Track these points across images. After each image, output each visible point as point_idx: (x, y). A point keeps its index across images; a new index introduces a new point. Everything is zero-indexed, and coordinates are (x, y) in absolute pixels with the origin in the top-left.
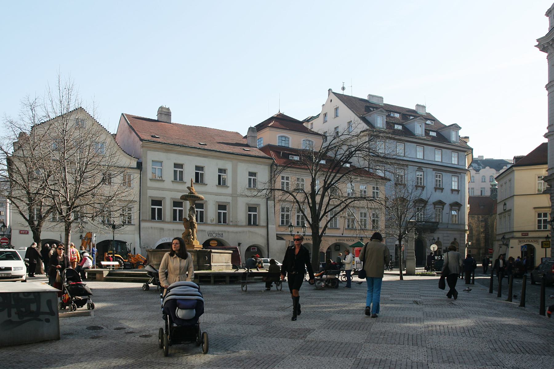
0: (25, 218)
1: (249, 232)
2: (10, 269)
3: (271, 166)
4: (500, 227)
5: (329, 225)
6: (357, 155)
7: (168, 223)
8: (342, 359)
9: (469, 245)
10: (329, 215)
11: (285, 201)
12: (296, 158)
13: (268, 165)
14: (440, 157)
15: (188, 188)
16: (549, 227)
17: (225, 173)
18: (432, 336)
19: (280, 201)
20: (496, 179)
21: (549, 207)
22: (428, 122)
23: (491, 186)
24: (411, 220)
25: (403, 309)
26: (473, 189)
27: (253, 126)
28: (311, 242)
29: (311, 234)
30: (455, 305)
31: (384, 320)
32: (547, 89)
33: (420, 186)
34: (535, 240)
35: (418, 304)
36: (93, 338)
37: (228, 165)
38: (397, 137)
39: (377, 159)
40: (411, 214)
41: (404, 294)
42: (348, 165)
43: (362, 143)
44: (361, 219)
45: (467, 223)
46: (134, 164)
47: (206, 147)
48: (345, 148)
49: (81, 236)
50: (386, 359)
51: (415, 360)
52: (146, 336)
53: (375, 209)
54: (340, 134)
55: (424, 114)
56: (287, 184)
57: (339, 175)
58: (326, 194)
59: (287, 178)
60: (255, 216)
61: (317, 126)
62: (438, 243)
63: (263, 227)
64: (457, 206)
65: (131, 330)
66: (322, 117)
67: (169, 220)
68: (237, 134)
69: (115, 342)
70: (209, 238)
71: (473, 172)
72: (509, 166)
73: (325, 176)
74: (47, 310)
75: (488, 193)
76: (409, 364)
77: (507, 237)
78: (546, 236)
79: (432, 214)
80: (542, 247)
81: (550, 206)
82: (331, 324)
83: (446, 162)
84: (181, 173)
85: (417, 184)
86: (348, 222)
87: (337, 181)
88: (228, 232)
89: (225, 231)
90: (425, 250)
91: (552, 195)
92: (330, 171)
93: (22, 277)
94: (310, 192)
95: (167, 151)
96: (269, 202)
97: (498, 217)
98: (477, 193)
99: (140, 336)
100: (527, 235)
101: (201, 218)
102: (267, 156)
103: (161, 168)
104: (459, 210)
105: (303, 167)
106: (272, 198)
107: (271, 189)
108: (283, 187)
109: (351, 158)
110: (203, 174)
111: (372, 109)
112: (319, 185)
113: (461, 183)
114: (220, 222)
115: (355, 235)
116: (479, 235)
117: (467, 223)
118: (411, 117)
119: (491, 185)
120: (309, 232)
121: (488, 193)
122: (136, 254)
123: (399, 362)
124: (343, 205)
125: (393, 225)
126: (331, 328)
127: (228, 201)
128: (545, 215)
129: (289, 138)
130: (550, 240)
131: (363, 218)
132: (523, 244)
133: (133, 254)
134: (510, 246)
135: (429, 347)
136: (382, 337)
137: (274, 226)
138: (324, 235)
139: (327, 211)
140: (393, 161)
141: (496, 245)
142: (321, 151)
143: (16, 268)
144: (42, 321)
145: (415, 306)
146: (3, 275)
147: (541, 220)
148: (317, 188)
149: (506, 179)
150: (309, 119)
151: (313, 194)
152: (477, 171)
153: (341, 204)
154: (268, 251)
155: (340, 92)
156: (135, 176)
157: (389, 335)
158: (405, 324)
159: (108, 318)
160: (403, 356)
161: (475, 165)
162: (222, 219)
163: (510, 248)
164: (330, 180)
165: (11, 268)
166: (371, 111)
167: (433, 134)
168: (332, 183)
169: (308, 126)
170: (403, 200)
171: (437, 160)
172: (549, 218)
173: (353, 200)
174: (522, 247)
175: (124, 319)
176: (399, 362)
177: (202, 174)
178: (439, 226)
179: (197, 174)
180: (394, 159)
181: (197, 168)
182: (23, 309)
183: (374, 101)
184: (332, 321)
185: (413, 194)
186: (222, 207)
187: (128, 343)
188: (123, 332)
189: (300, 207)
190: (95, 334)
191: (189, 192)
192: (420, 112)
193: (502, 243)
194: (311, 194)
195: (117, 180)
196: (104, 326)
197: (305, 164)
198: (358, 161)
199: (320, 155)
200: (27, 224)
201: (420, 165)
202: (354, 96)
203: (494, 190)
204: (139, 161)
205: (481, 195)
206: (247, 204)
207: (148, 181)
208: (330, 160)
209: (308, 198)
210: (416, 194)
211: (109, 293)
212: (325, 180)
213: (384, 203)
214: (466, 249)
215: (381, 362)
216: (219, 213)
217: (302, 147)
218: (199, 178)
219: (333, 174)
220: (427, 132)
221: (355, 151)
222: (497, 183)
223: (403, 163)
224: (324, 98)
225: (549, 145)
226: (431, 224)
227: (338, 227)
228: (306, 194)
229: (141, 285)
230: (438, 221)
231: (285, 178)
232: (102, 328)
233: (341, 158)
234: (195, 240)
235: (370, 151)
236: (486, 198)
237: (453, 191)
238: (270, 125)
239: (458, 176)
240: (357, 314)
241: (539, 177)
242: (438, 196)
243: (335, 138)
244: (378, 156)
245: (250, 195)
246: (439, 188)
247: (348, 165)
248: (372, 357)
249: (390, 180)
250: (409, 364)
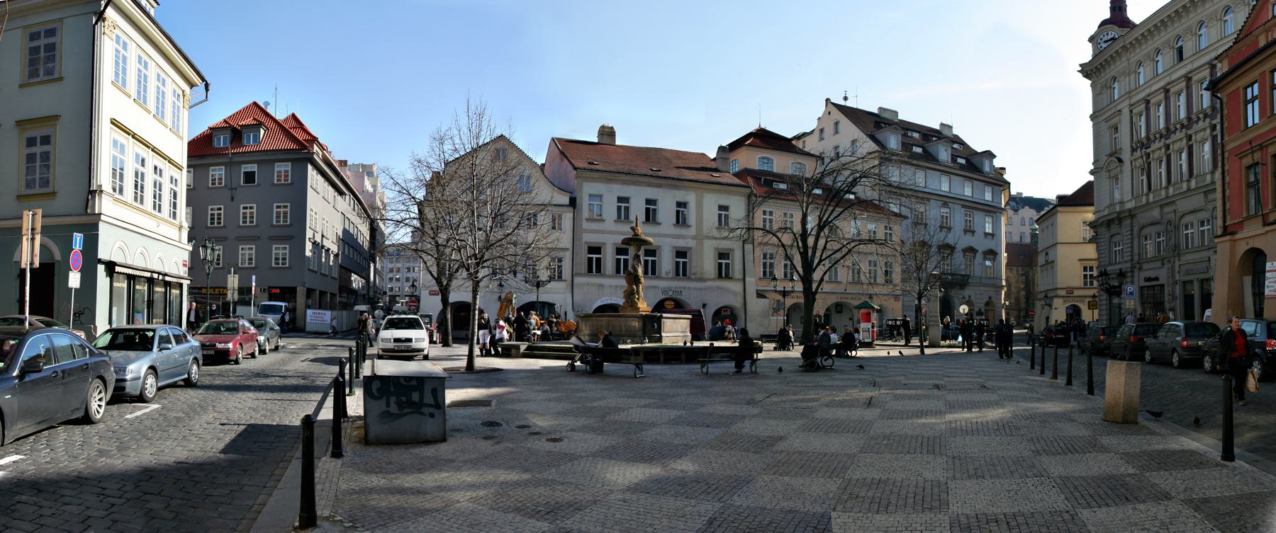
0: (432, 275)
1: (719, 288)
2: (410, 340)
3: (749, 197)
4: (1042, 284)
5: (826, 278)
6: (862, 183)
7: (609, 277)
8: (822, 480)
9: (1006, 306)
10: (827, 263)
11: (766, 244)
12: (783, 186)
13: (745, 196)
14: (971, 190)
15: (633, 229)
16: (1095, 283)
17: (685, 207)
18: (955, 437)
19: (760, 244)
20: (1036, 221)
21: (1095, 260)
22: (956, 146)
23: (1030, 231)
24: (933, 273)
25: (917, 398)
26: (1010, 233)
27: (724, 144)
28: (802, 301)
29: (802, 290)
30: (988, 389)
31: (891, 416)
32: (1092, 120)
33: (945, 227)
34: (1082, 299)
35: (939, 389)
36: (486, 438)
37: (690, 197)
38: (915, 162)
39: (888, 189)
40: (934, 264)
41: (923, 374)
42: (852, 197)
43: (868, 167)
44: (870, 270)
45: (1004, 277)
46: (566, 200)
47: (660, 174)
48: (847, 173)
49: (500, 297)
50: (888, 478)
51: (930, 478)
52: (555, 440)
53: (887, 256)
54: (840, 155)
55: (950, 135)
56: (771, 221)
57: (839, 210)
58: (822, 234)
59: (771, 213)
60: (727, 265)
61: (811, 145)
62: (969, 303)
63: (738, 280)
64: (992, 254)
65: (537, 430)
66: (817, 134)
67: (611, 273)
68: (703, 155)
69: (511, 446)
70: (663, 297)
71: (1011, 212)
72: (1051, 207)
73: (819, 210)
74: (431, 401)
75: (1027, 240)
76: (921, 485)
77: (1049, 295)
78: (1092, 295)
79: (960, 265)
80: (1089, 308)
81: (1096, 258)
82: (815, 423)
83: (977, 198)
84: (627, 209)
85: (942, 223)
86: (853, 273)
87: (836, 217)
89: (685, 288)
90: (954, 312)
91: (1099, 245)
92: (827, 203)
93: (423, 350)
94: (801, 232)
95: (609, 181)
96: (745, 246)
97: (1039, 269)
98: (1016, 239)
99: (547, 440)
100: (1073, 293)
101: (652, 270)
102: (743, 183)
103: (600, 203)
104: (994, 260)
105: (790, 198)
106: (751, 239)
107: (749, 229)
108: (764, 226)
109: (854, 187)
111: (883, 125)
112: (812, 223)
113: (996, 225)
114: (678, 274)
115: (861, 292)
116: (1018, 292)
117: (1004, 277)
118: (934, 139)
119: (1031, 229)
120: (799, 287)
121: (1027, 240)
122: (567, 319)
123: (906, 483)
124: (845, 250)
125: (911, 279)
126: (813, 430)
127: (689, 246)
128: (1091, 269)
129: (772, 160)
130: (1097, 299)
131: (873, 268)
132: (1068, 305)
133: (564, 320)
134: (1053, 308)
135: (951, 455)
136: (885, 442)
137: (753, 279)
138: (820, 290)
139: (823, 258)
140: (910, 193)
141: (1038, 304)
142: (814, 177)
143: (418, 340)
144: (425, 415)
145: (936, 392)
146: (403, 348)
147: (1090, 271)
148: (809, 226)
149: (1048, 223)
150: (800, 136)
151: (804, 235)
152: (1016, 211)
153: (841, 248)
154: (746, 314)
155: (842, 103)
157: (896, 438)
158: (919, 421)
159: (513, 410)
160: (913, 471)
161: (1013, 203)
162: (681, 271)
163: (1053, 310)
164: (826, 216)
165: (411, 339)
166: (882, 128)
167: (962, 161)
168: (830, 220)
169: (799, 144)
170: (924, 244)
171: (966, 194)
172: (1095, 273)
173: (857, 243)
174: (1067, 308)
175: (533, 412)
176: (906, 483)
177: (654, 210)
178: (970, 281)
179: (647, 210)
180: (911, 190)
181: (649, 202)
182: (404, 399)
183: (887, 116)
184: (817, 419)
185: (935, 237)
186: (681, 253)
187: (529, 449)
188: (526, 431)
189: (786, 254)
190: (489, 433)
191: (633, 233)
192: (946, 132)
193: (1044, 303)
194: (801, 235)
195: (544, 219)
196: (505, 422)
197: (793, 195)
198: (865, 190)
199: (813, 183)
200: (434, 281)
201: (946, 200)
202: (859, 108)
203: (1034, 236)
205: (1021, 241)
206: (717, 249)
207: (584, 221)
208: (827, 189)
209: (797, 240)
210: (940, 237)
211: (522, 374)
212: (819, 216)
213: (899, 249)
214: (1003, 311)
215: (880, 483)
216: (678, 263)
217: (790, 172)
218: (650, 216)
219: (831, 208)
220: (954, 158)
221: (860, 177)
222: (1037, 227)
223: (924, 196)
224: (820, 109)
225: (1095, 184)
226: (960, 277)
227: (839, 280)
228: (794, 235)
229: (565, 363)
230: (968, 273)
231: (768, 213)
232: (501, 425)
233: (841, 186)
234: (641, 299)
235: (881, 178)
236: (1026, 245)
237: (986, 234)
238: (746, 143)
239: (993, 217)
240: (854, 407)
241: (1084, 223)
242: (966, 241)
243: (832, 160)
244: (890, 185)
245: (719, 236)
246: (969, 231)
247: (852, 197)
248: (868, 475)
249: (906, 218)
250: (921, 485)
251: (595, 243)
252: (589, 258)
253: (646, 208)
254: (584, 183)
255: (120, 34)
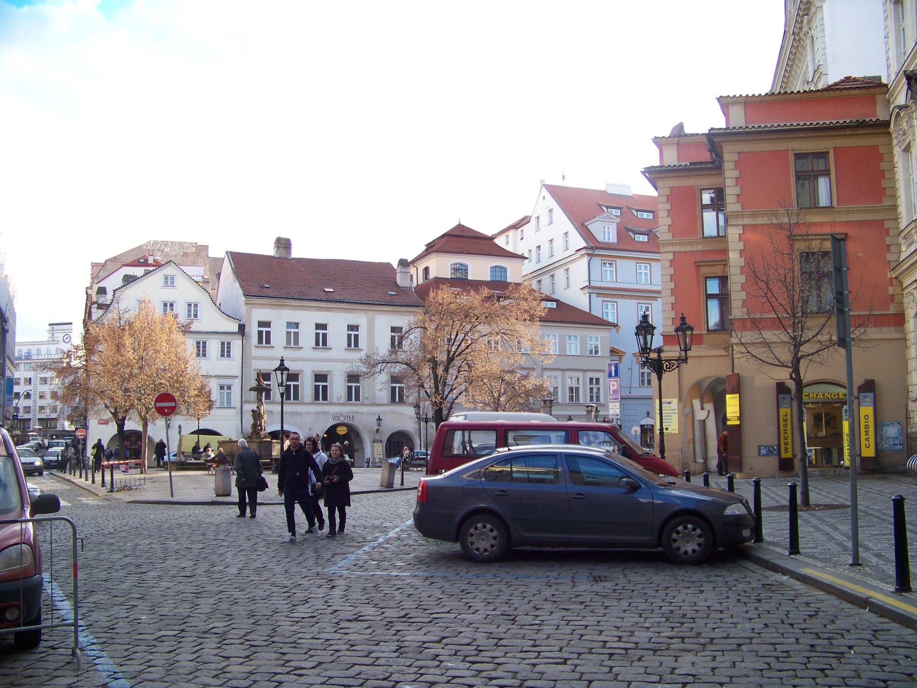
1: (392, 412)
46: (235, 328)
88: (362, 413)
110: (358, 335)
156: (236, 345)
169: (500, 242)
204: (241, 323)
227: (232, 405)
251: (323, 371)
252: (392, 387)
253: (348, 335)
254: (253, 310)
255: (789, 414)
